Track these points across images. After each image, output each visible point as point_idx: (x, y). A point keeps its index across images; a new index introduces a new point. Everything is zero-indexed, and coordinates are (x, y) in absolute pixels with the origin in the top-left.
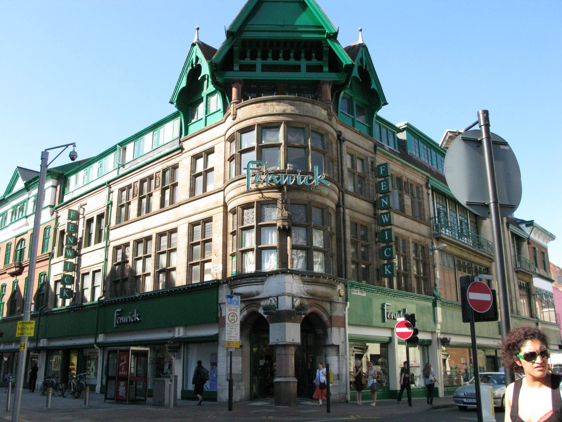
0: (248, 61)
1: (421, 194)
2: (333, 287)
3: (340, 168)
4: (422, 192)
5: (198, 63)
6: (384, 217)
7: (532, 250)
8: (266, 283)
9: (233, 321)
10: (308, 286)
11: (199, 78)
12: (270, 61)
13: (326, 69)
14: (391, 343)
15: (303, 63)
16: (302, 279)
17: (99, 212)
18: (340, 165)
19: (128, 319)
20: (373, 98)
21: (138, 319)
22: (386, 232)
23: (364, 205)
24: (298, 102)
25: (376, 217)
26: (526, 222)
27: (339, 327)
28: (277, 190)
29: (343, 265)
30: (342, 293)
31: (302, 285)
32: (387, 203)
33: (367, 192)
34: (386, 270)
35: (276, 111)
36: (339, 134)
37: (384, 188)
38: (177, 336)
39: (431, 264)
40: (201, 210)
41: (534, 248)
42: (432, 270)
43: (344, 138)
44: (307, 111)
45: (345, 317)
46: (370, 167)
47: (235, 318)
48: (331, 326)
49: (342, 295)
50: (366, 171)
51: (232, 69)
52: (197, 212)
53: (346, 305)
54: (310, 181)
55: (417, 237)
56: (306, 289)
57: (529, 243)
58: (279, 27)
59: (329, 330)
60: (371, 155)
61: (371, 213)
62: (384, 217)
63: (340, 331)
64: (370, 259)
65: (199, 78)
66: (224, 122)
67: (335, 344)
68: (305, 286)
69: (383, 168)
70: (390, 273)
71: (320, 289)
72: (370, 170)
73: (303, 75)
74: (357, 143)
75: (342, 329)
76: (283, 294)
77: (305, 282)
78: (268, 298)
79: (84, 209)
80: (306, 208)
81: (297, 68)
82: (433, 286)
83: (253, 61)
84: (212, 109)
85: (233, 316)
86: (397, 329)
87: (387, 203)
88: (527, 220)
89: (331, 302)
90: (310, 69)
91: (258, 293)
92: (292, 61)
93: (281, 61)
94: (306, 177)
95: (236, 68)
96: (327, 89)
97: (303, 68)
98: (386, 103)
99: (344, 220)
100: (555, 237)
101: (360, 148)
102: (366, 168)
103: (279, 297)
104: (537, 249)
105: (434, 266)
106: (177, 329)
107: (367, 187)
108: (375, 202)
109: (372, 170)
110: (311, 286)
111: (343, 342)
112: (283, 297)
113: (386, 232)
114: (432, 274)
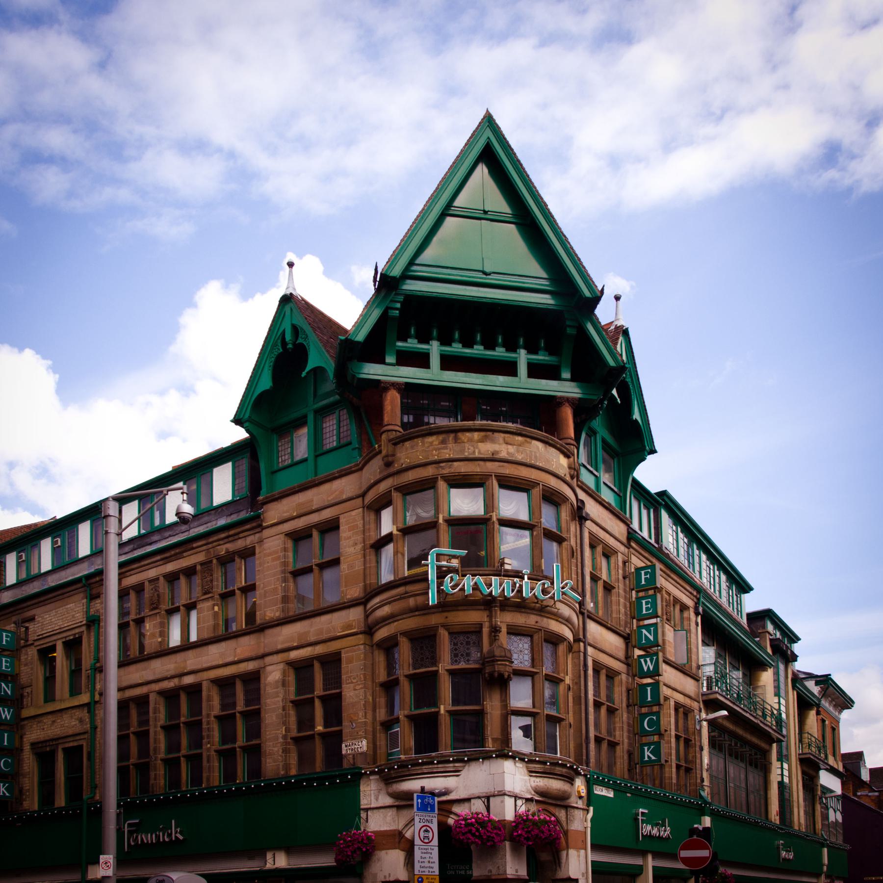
0: (412, 344)
1: (686, 623)
2: (571, 781)
3: (580, 571)
4: (689, 619)
5: (300, 341)
6: (646, 662)
7: (820, 723)
8: (462, 773)
9: (426, 841)
10: (538, 780)
11: (304, 374)
12: (457, 348)
13: (566, 375)
14: (642, 876)
15: (523, 358)
16: (527, 768)
17: (70, 636)
18: (579, 564)
19: (158, 837)
20: (630, 440)
21: (181, 838)
22: (649, 689)
23: (613, 642)
24: (520, 438)
25: (628, 660)
26: (817, 676)
27: (578, 849)
28: (483, 607)
29: (584, 745)
30: (584, 793)
31: (527, 778)
32: (651, 638)
33: (614, 615)
34: (647, 753)
35: (480, 453)
36: (581, 505)
37: (647, 609)
38: (269, 865)
39: (698, 744)
40: (313, 639)
41: (823, 721)
42: (698, 755)
43: (587, 514)
44: (536, 457)
45: (585, 833)
46: (621, 571)
47: (430, 835)
48: (568, 848)
49: (583, 795)
50: (613, 578)
51: (382, 361)
52: (303, 642)
53: (588, 811)
54: (545, 592)
55: (680, 698)
56: (533, 784)
57: (818, 713)
58: (480, 275)
59: (564, 853)
60: (622, 548)
61: (621, 654)
62: (646, 662)
63: (579, 856)
64: (617, 733)
65: (304, 374)
66: (361, 469)
67: (573, 877)
68: (533, 779)
69: (646, 574)
70: (653, 758)
71: (556, 785)
72: (621, 577)
73: (523, 383)
74: (603, 525)
75: (582, 852)
76: (503, 794)
77: (531, 772)
78: (468, 800)
79: (27, 628)
80: (532, 641)
81: (510, 369)
82: (699, 781)
83: (424, 346)
84: (331, 441)
85: (426, 831)
86: (682, 852)
87: (651, 638)
88: (819, 674)
89: (567, 807)
90: (535, 371)
91: (447, 792)
92: (500, 352)
93: (478, 350)
94: (539, 586)
95: (391, 359)
96: (568, 414)
97: (523, 369)
98: (653, 451)
99: (586, 665)
100: (853, 702)
101: (607, 535)
102: (613, 573)
103: (491, 799)
104: (827, 722)
105: (702, 749)
106: (269, 856)
107: (614, 607)
108: (629, 634)
109: (624, 578)
110: (541, 779)
111: (583, 874)
112: (498, 799)
113: (649, 689)
114: (698, 761)
